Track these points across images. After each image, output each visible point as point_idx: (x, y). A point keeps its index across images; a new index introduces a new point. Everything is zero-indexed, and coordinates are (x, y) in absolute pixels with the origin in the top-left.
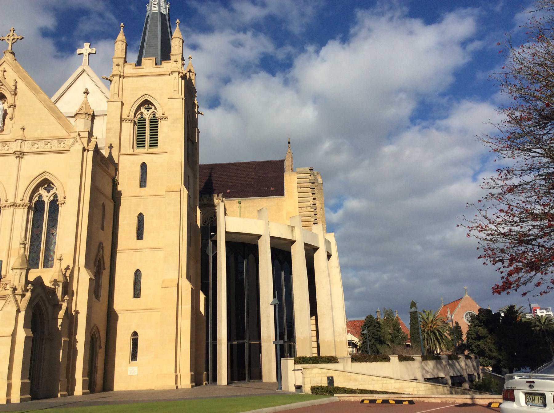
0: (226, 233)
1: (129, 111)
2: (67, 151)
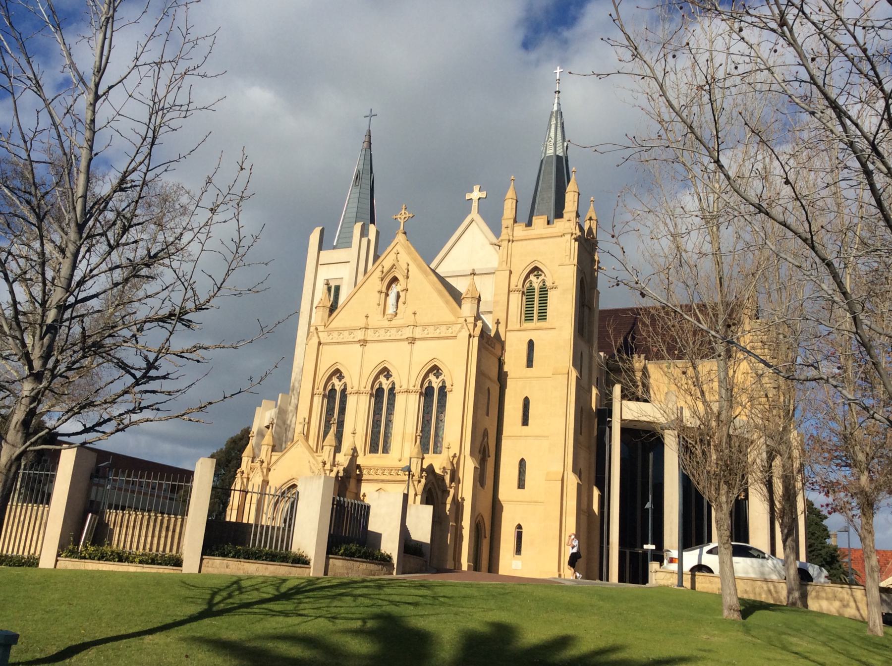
0: (622, 420)
1: (517, 281)
2: (455, 337)
